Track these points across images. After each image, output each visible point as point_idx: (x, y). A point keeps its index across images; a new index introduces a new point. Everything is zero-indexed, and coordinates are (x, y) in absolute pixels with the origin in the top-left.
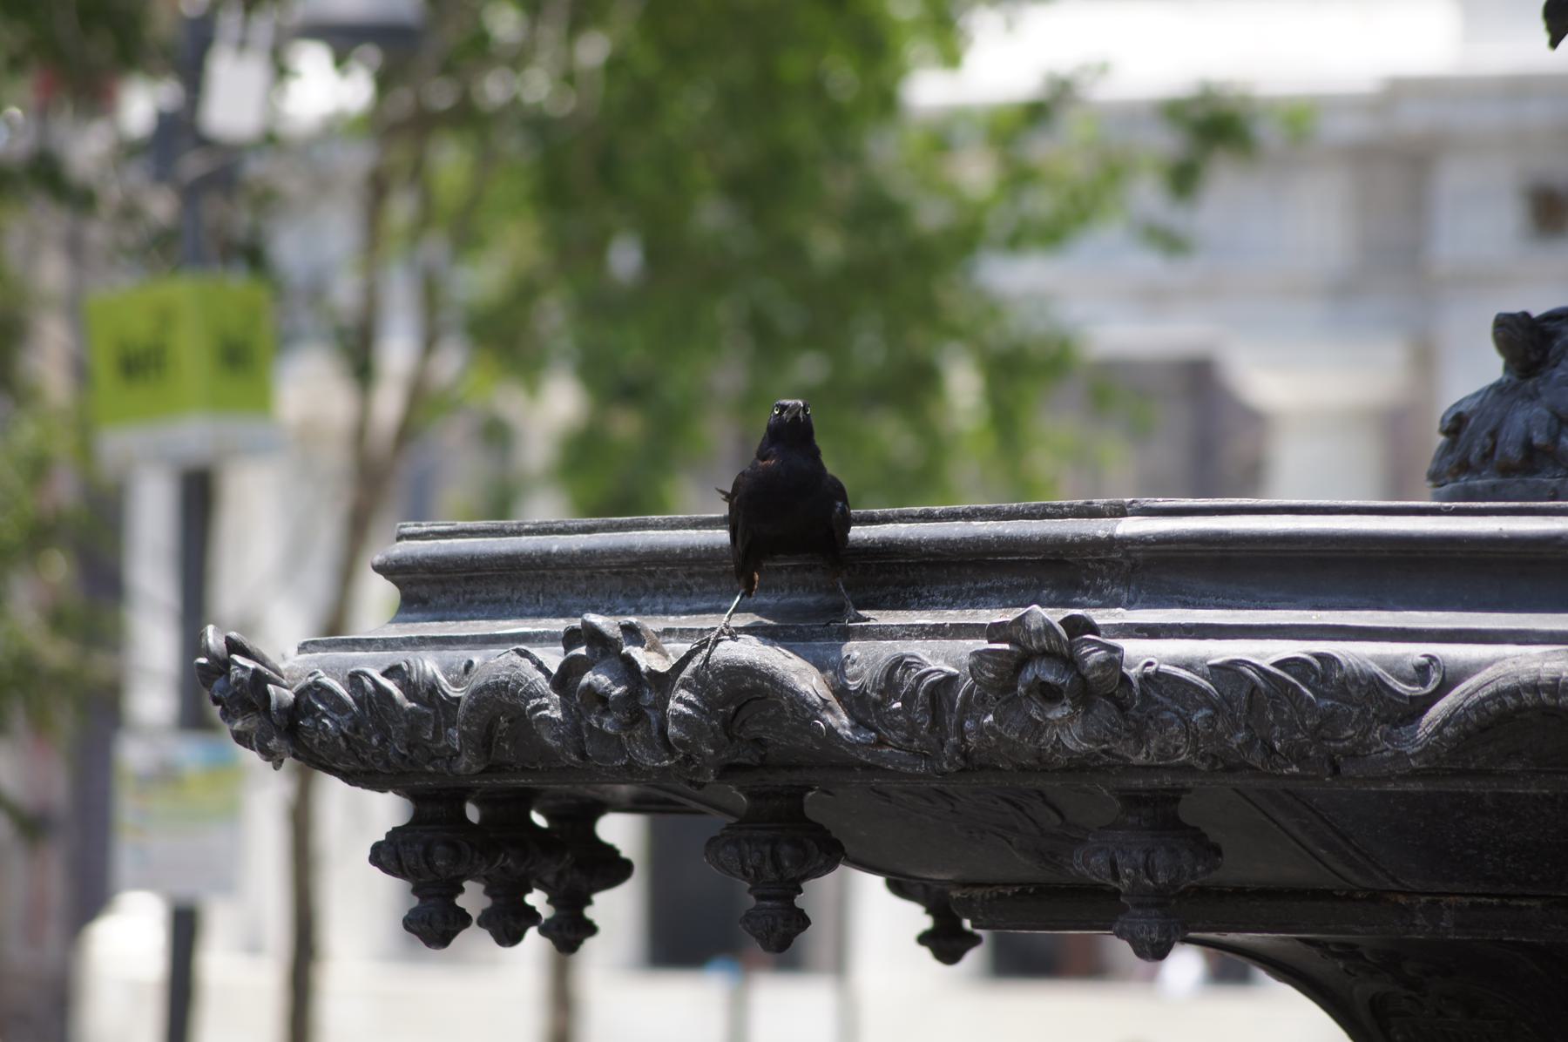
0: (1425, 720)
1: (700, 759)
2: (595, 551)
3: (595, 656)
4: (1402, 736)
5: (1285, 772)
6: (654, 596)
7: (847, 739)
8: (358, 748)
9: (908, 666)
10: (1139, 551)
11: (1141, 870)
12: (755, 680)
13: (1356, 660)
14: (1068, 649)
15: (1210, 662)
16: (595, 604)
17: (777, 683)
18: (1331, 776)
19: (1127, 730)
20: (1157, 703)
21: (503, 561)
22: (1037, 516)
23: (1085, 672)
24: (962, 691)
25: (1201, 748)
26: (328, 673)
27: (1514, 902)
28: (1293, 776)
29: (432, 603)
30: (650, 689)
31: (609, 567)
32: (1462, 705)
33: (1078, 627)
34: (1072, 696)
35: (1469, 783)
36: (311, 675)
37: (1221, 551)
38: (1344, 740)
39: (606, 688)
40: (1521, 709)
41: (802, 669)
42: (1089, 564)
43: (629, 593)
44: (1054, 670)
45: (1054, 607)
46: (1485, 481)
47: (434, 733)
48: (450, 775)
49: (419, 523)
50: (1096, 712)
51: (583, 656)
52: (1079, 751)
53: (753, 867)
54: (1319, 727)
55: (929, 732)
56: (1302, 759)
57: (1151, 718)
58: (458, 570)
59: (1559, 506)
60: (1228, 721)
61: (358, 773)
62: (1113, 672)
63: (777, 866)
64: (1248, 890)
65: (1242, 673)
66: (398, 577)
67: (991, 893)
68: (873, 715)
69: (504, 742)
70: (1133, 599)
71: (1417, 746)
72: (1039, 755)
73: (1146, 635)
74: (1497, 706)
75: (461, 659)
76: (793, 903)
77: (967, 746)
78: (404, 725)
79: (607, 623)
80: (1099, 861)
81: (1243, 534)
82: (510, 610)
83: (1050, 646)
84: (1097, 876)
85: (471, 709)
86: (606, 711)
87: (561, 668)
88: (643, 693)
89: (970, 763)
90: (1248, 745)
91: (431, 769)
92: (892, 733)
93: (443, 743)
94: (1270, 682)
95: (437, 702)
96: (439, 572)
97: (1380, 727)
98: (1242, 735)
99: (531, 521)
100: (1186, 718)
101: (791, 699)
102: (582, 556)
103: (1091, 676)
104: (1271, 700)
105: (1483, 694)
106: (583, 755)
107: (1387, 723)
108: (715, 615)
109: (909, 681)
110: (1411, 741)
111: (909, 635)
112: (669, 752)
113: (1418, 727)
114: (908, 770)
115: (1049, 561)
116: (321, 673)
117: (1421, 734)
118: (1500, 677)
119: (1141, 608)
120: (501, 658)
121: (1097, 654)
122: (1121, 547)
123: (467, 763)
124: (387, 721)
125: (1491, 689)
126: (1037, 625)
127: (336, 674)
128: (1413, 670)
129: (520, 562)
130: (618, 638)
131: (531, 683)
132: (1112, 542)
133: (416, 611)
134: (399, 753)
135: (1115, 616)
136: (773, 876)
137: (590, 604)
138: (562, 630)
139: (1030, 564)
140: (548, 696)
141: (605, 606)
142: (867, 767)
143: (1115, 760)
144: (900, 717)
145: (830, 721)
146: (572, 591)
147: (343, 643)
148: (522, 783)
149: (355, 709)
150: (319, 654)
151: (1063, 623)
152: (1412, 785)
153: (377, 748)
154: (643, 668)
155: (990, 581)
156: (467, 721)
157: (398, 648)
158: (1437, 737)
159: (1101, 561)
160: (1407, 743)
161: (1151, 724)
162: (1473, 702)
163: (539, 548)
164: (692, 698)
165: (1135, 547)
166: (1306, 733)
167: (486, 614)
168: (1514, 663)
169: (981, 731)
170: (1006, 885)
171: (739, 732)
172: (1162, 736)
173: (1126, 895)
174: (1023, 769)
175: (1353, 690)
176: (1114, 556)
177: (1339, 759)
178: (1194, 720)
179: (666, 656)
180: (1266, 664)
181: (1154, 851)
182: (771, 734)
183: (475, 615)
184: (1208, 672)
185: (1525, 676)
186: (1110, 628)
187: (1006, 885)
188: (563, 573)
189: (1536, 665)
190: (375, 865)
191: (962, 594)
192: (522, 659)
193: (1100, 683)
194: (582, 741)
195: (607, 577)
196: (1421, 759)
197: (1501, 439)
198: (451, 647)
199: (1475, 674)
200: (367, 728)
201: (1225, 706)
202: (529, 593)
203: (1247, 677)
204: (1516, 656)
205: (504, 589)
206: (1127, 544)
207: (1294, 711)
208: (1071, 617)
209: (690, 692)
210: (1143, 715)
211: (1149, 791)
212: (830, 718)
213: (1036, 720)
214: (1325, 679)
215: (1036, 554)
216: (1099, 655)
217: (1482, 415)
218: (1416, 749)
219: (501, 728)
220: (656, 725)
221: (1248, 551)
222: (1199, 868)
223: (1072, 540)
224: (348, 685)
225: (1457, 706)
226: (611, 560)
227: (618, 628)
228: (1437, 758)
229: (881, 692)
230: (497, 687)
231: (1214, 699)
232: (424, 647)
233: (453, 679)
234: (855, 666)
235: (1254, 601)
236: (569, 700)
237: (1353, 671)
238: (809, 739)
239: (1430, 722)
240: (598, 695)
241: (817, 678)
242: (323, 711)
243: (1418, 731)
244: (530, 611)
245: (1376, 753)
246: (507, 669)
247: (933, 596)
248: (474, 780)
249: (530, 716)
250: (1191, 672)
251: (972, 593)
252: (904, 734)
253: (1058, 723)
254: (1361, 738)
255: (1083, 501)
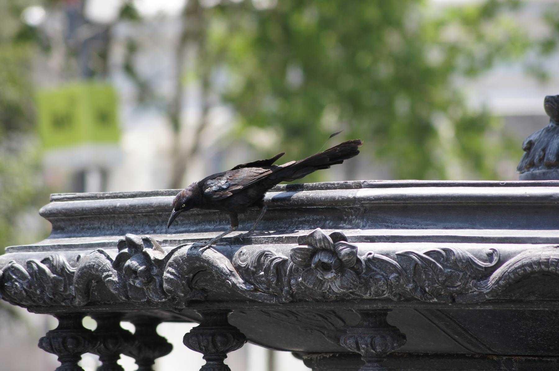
0: (491, 277)
1: (178, 298)
2: (135, 206)
3: (132, 253)
4: (482, 285)
5: (431, 301)
6: (162, 225)
7: (241, 289)
8: (31, 295)
9: (266, 256)
10: (367, 204)
11: (369, 346)
12: (204, 263)
13: (461, 252)
14: (333, 247)
15: (397, 253)
16: (137, 229)
17: (210, 264)
18: (451, 303)
19: (361, 283)
20: (374, 271)
21: (96, 210)
22: (324, 188)
23: (341, 257)
24: (289, 266)
25: (394, 291)
26: (18, 262)
27: (544, 359)
28: (435, 303)
29: (66, 230)
30: (156, 267)
31: (141, 213)
32: (507, 271)
33: (337, 237)
34: (335, 268)
35: (513, 305)
36: (10, 263)
37: (403, 203)
38: (456, 287)
39: (136, 267)
40: (533, 272)
41: (221, 257)
42: (346, 209)
43: (151, 224)
44: (327, 257)
45: (331, 229)
46: (540, 171)
47: (64, 288)
48: (72, 307)
49: (60, 194)
50: (346, 275)
51: (126, 253)
52: (339, 293)
53: (204, 346)
54: (445, 281)
55: (276, 285)
56: (438, 296)
57: (371, 278)
58: (76, 215)
59: (551, 182)
60: (405, 279)
61: (33, 307)
62: (353, 258)
63: (215, 346)
64: (430, 354)
65: (411, 257)
66: (51, 218)
67: (320, 356)
68: (252, 278)
69: (95, 292)
70: (365, 225)
71: (488, 289)
72: (323, 295)
73: (369, 241)
74: (522, 271)
75: (76, 255)
76: (223, 362)
77: (292, 291)
78: (51, 285)
79: (137, 238)
80: (351, 342)
81: (413, 196)
82: (100, 232)
83: (325, 246)
84: (350, 349)
85: (79, 277)
86: (136, 278)
87: (117, 258)
88: (153, 269)
89: (295, 299)
90: (415, 289)
91: (64, 304)
92: (261, 286)
93: (68, 293)
94: (423, 262)
95: (65, 274)
96: (69, 215)
97: (472, 281)
98: (411, 285)
99: (108, 192)
100: (387, 278)
101: (216, 271)
102: (130, 208)
103: (344, 259)
104: (424, 269)
105: (516, 266)
106: (127, 297)
107: (475, 279)
108: (187, 234)
109: (267, 262)
110: (486, 287)
111: (268, 242)
112: (165, 295)
113: (488, 281)
114: (268, 302)
115: (329, 208)
116: (14, 262)
117: (490, 284)
118: (524, 258)
119: (368, 229)
120: (91, 254)
121: (345, 250)
122: (359, 202)
123: (79, 301)
124: (43, 283)
125: (519, 264)
126: (319, 237)
127: (21, 262)
128: (486, 256)
129: (103, 211)
130: (141, 245)
131: (104, 265)
132: (355, 200)
133: (59, 233)
134: (49, 297)
135: (356, 232)
136: (213, 350)
137: (134, 229)
138: (118, 241)
139: (321, 210)
140: (112, 271)
141: (141, 230)
142: (251, 301)
143: (356, 297)
144: (263, 279)
145: (233, 280)
146: (127, 224)
147: (25, 248)
148: (104, 310)
149: (29, 278)
150: (14, 253)
151: (331, 236)
152: (487, 307)
153: (39, 295)
154: (152, 258)
155: (304, 217)
156: (77, 283)
157: (49, 250)
158: (497, 285)
159: (351, 208)
160: (484, 288)
161: (371, 280)
162: (512, 269)
163: (111, 205)
164: (173, 271)
165: (365, 202)
166: (440, 284)
167: (89, 235)
168: (530, 252)
169: (298, 284)
170: (326, 353)
171: (195, 286)
172: (376, 286)
173: (364, 357)
174: (317, 301)
175: (460, 264)
176: (356, 206)
177: (455, 295)
178: (390, 278)
179: (163, 252)
180: (421, 254)
181: (375, 337)
182: (209, 287)
183: (84, 235)
184: (396, 257)
185: (534, 258)
186: (353, 238)
187: (326, 353)
188: (122, 215)
189: (539, 253)
190: (41, 348)
191: (293, 223)
192: (100, 254)
193: (348, 262)
194: (127, 291)
195: (141, 217)
196: (490, 295)
197: (547, 152)
198: (72, 249)
199: (513, 257)
200: (35, 286)
201: (404, 272)
202: (108, 225)
203: (413, 259)
204: (532, 249)
205: (97, 223)
206: (362, 201)
207: (434, 274)
208: (334, 233)
209: (173, 268)
210: (368, 276)
211: (373, 310)
212: (233, 279)
213: (320, 279)
214: (447, 260)
215: (325, 205)
216: (347, 250)
217: (539, 142)
218: (488, 291)
219: (93, 285)
220: (158, 284)
221: (414, 203)
222: (395, 345)
223: (338, 199)
224: (26, 267)
225: (505, 271)
226: (143, 210)
227: (141, 240)
228: (497, 295)
229: (255, 267)
230: (90, 267)
231: (398, 269)
232: (60, 250)
233: (72, 264)
234: (244, 256)
235: (418, 225)
236: (120, 272)
237: (459, 257)
238: (225, 289)
239: (493, 279)
240: (133, 270)
241: (228, 261)
242: (15, 279)
243: (489, 283)
244: (108, 232)
245: (471, 292)
246: (94, 259)
247: (280, 224)
248: (83, 309)
249: (104, 280)
250: (389, 257)
251: (297, 223)
252: (265, 286)
253: (330, 280)
254: (464, 286)
255: (343, 181)
